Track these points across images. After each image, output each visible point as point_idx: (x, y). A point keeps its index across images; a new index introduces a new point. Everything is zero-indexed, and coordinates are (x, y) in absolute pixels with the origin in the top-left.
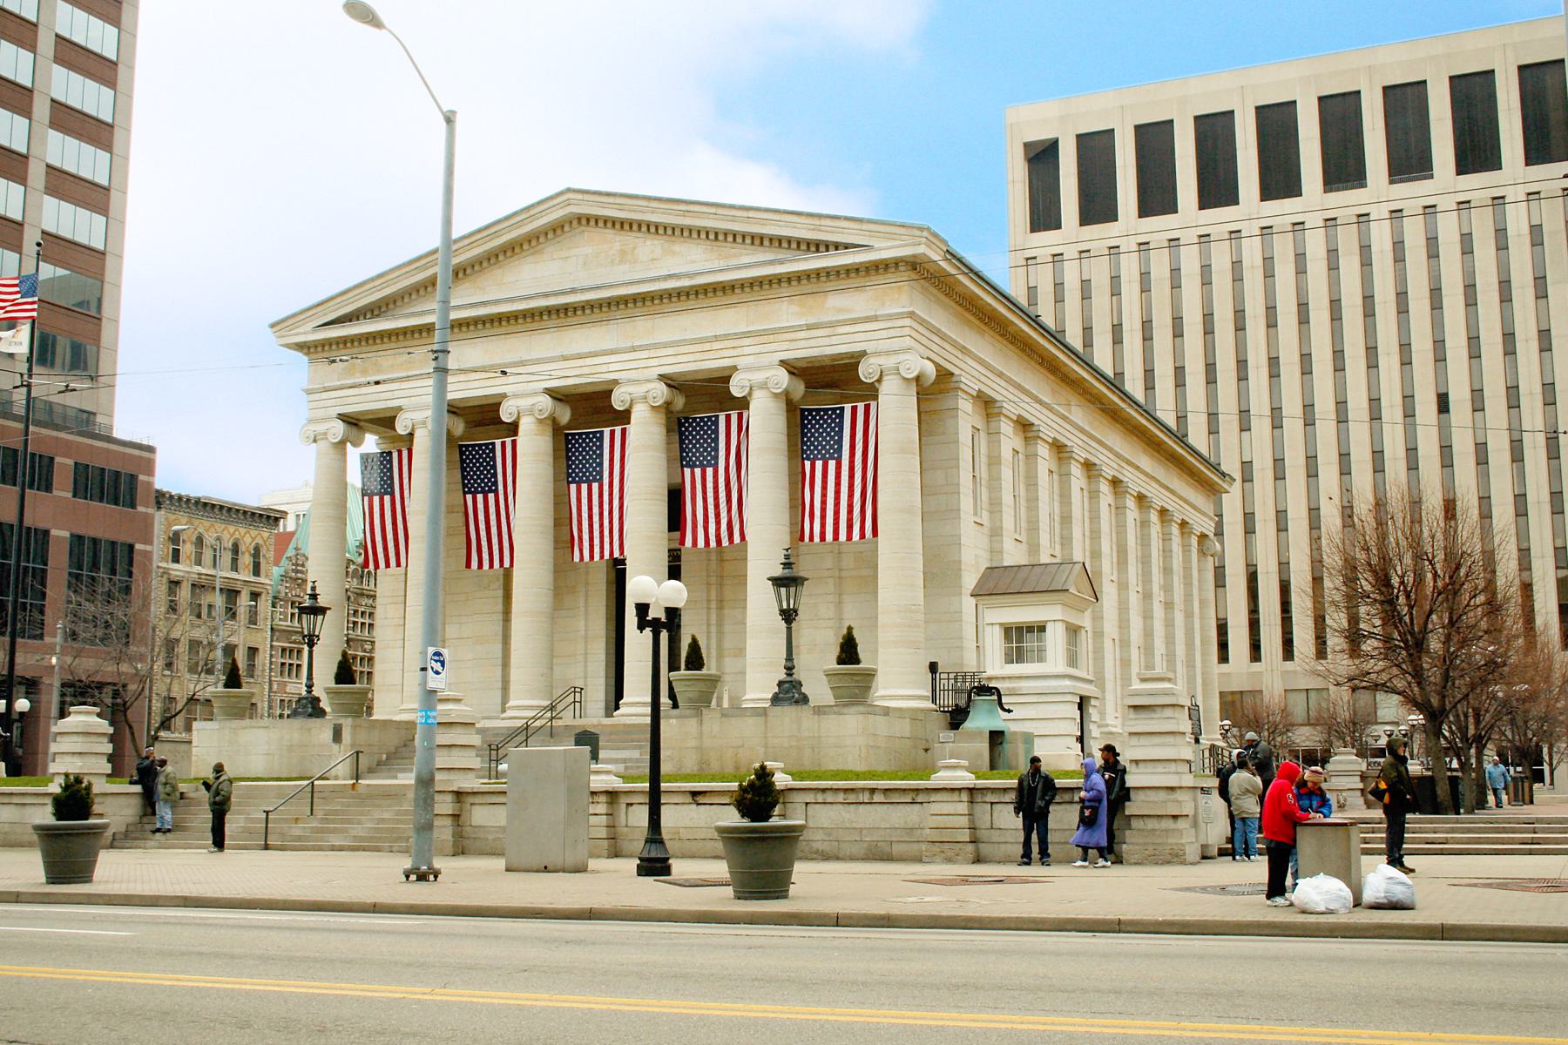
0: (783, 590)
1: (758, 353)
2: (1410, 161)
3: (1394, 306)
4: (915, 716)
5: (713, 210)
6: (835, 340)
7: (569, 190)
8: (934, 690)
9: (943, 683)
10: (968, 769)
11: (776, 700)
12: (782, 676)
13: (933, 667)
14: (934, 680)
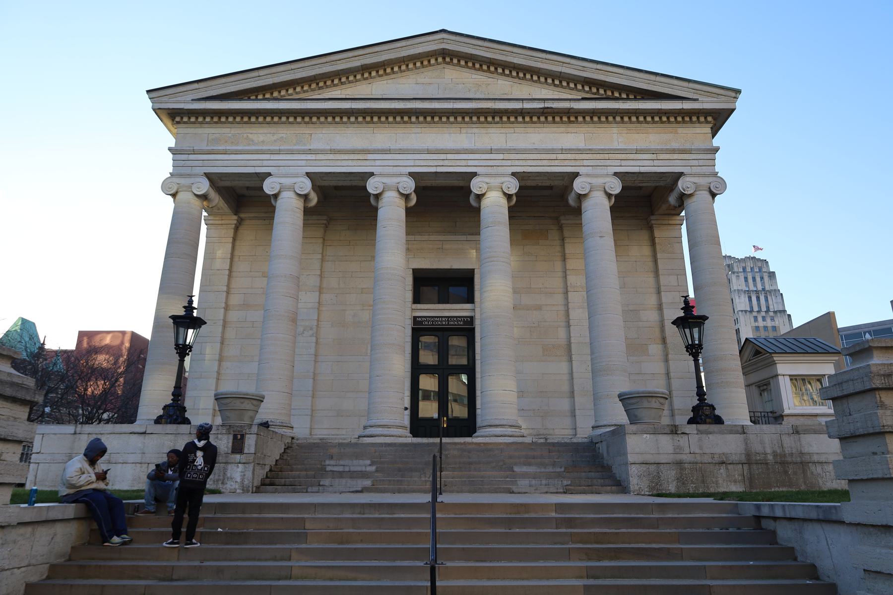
6: (656, 163)
7: (443, 31)
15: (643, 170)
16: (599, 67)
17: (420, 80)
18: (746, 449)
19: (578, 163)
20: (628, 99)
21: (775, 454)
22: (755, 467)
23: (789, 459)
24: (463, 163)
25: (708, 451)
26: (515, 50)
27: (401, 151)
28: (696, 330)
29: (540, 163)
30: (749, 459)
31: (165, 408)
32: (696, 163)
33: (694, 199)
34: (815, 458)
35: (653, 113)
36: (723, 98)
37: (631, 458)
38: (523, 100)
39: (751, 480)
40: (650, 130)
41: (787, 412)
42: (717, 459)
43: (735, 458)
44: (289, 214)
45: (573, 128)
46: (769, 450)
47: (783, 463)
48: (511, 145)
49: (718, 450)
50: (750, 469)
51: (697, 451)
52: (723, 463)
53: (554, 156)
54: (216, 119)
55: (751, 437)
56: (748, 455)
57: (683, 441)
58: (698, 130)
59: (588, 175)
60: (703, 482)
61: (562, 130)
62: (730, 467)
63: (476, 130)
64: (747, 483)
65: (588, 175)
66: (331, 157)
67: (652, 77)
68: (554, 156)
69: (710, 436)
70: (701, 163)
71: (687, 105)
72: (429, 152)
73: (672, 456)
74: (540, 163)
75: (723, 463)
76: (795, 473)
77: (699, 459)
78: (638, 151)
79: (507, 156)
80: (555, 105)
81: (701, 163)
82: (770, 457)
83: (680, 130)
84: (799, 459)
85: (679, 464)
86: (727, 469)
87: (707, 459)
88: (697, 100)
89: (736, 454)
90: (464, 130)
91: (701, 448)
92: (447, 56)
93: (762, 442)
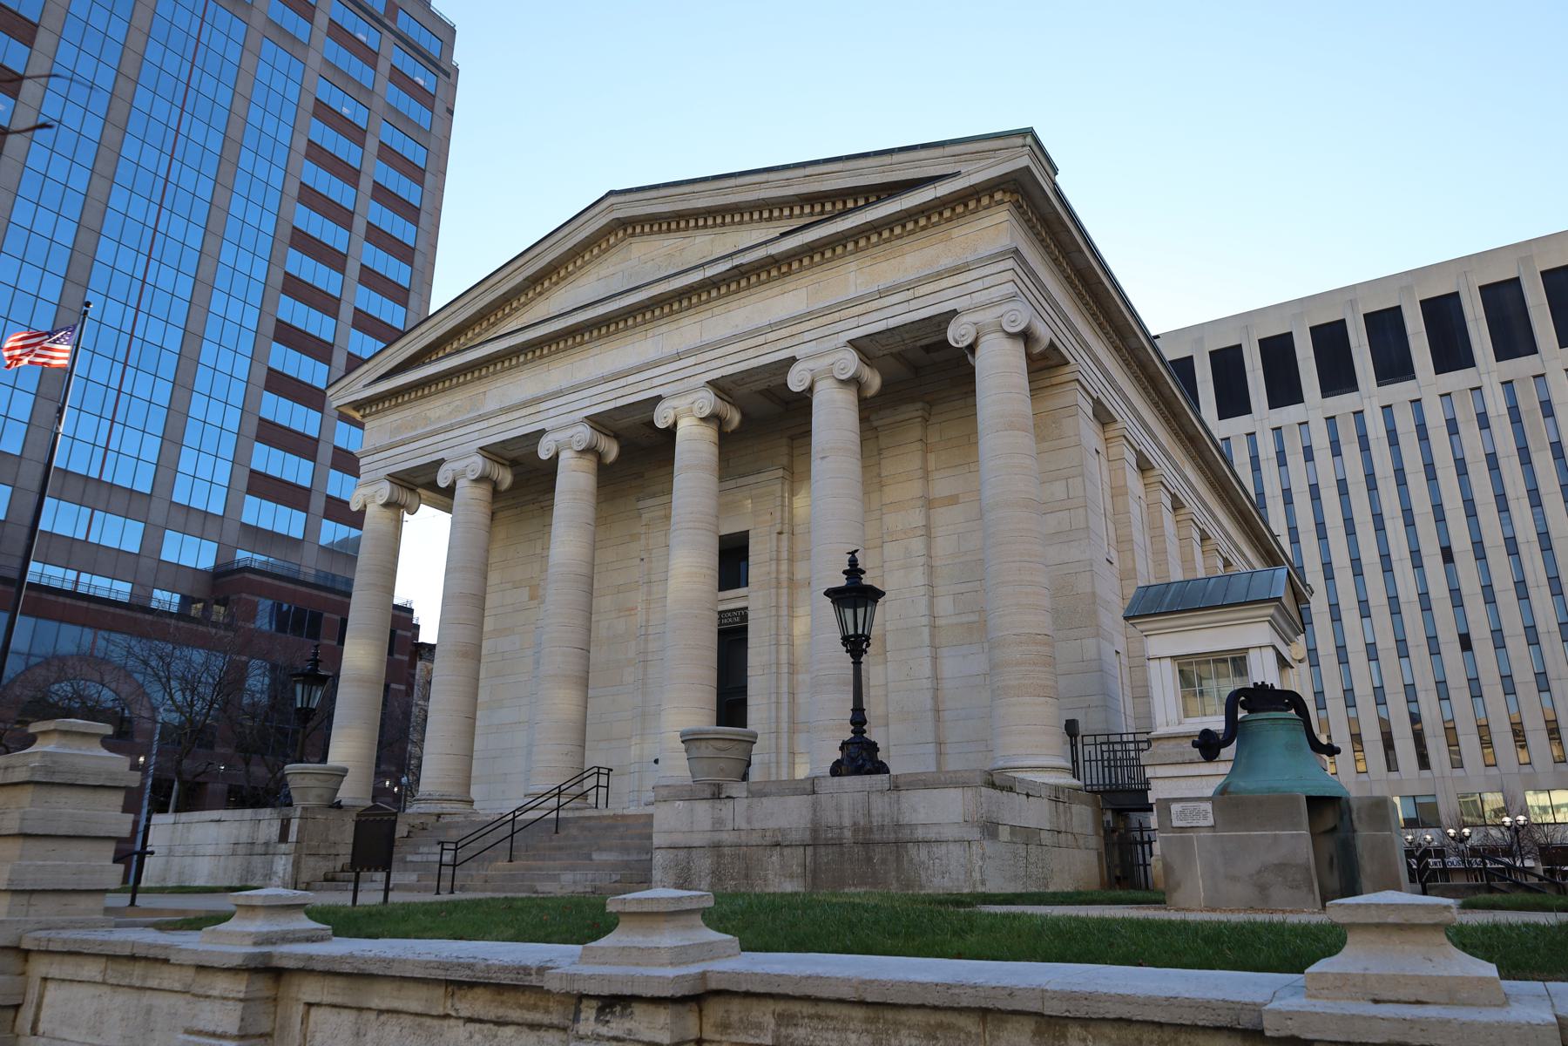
0: (849, 613)
1: (812, 330)
2: (1451, 352)
3: (1401, 521)
4: (1058, 796)
5: (764, 177)
6: (914, 304)
7: (611, 193)
8: (1075, 761)
9: (1088, 751)
10: (714, 919)
11: (837, 770)
12: (848, 735)
13: (1071, 728)
14: (1073, 746)
15: (892, 323)
16: (809, 171)
17: (603, 273)
18: (813, 821)
19: (796, 340)
20: (868, 204)
21: (856, 827)
22: (822, 850)
23: (877, 837)
24: (647, 384)
25: (757, 826)
26: (697, 187)
27: (576, 389)
28: (861, 611)
29: (743, 356)
30: (817, 839)
31: (844, 746)
32: (978, 285)
33: (979, 352)
34: (920, 834)
35: (925, 210)
36: (1004, 154)
37: (657, 840)
38: (702, 265)
39: (815, 873)
40: (907, 248)
41: (1160, 730)
42: (769, 840)
43: (795, 837)
44: (834, 419)
45: (791, 283)
46: (847, 822)
47: (867, 844)
48: (709, 337)
49: (771, 824)
50: (815, 854)
51: (744, 826)
52: (777, 845)
53: (761, 340)
54: (960, 209)
55: (823, 798)
56: (815, 831)
57: (726, 809)
58: (986, 222)
59: (809, 357)
60: (747, 876)
61: (776, 290)
62: (787, 851)
63: (664, 328)
64: (809, 879)
65: (809, 357)
66: (503, 418)
67: (886, 159)
68: (761, 340)
69: (764, 800)
70: (988, 282)
71: (943, 189)
72: (606, 380)
73: (708, 835)
74: (743, 356)
75: (777, 845)
76: (884, 861)
77: (744, 838)
78: (881, 294)
79: (701, 358)
80: (774, 249)
81: (988, 282)
82: (848, 834)
83: (956, 232)
84: (892, 837)
85: (717, 846)
86: (782, 855)
87: (755, 839)
88: (959, 173)
89: (797, 829)
90: (650, 333)
91: (749, 821)
92: (627, 227)
93: (838, 808)
